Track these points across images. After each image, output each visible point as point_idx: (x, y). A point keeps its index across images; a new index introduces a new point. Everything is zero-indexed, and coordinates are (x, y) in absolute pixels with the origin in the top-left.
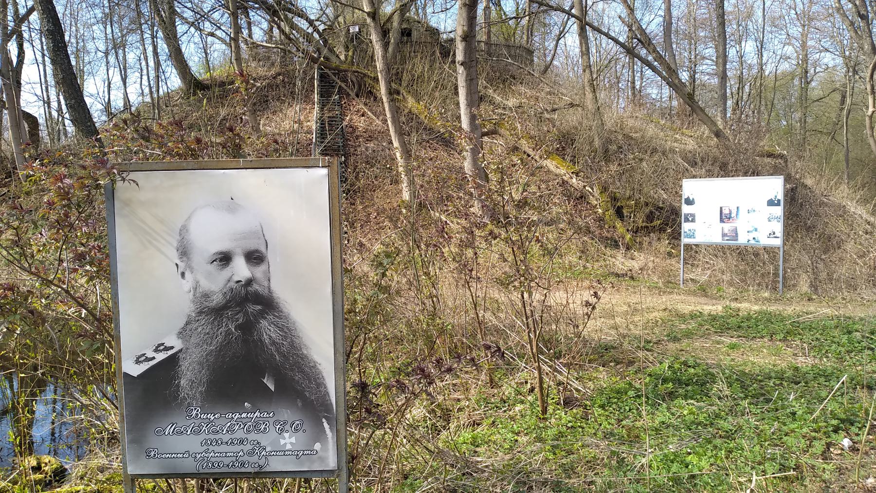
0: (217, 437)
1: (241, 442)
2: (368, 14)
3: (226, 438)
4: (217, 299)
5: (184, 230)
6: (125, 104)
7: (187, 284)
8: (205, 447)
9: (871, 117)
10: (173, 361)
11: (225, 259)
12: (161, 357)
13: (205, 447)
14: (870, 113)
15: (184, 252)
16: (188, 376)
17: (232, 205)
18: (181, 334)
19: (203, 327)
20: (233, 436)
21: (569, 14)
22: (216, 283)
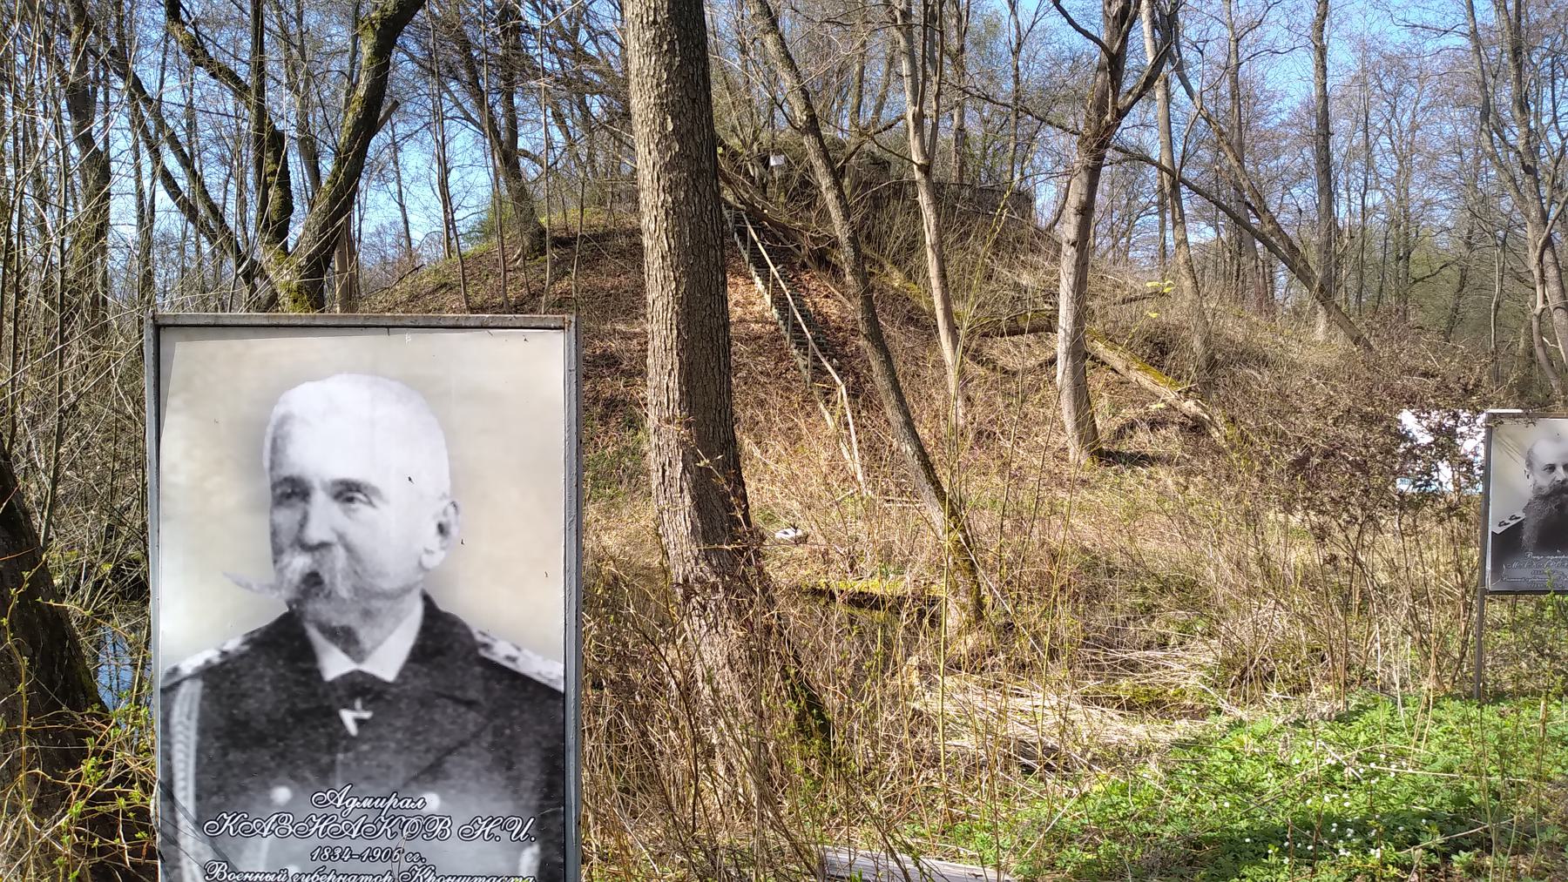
0: (344, 843)
1: (389, 855)
2: (920, 167)
3: (360, 846)
4: (1546, 491)
5: (1530, 452)
6: (519, 310)
7: (1530, 482)
8: (319, 863)
9: (1539, 317)
10: (1520, 525)
11: (1552, 468)
12: (1513, 522)
13: (319, 863)
14: (1538, 311)
15: (1530, 464)
16: (1527, 535)
17: (1558, 438)
18: (1525, 510)
19: (1538, 505)
20: (373, 844)
21: (1042, 120)
22: (1545, 482)
